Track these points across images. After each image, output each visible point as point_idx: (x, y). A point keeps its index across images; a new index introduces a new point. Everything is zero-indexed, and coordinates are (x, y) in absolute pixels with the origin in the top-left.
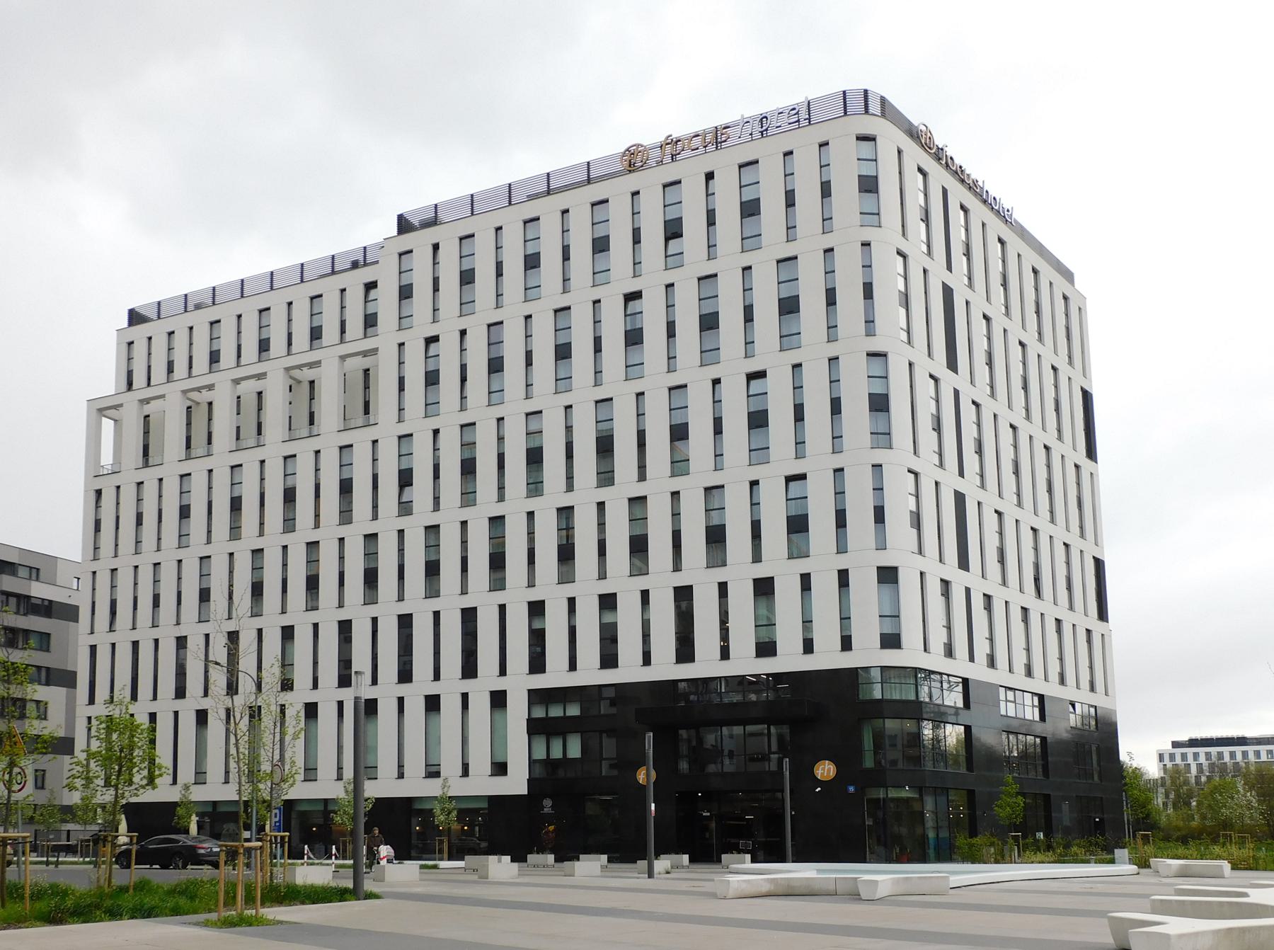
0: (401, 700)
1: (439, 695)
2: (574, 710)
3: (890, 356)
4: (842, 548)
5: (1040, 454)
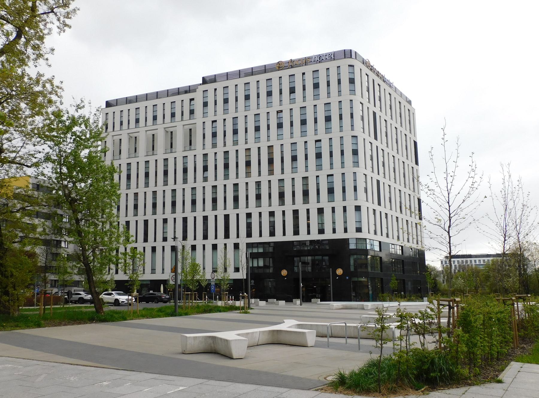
0: (204, 246)
1: (217, 244)
2: (261, 250)
3: (358, 137)
4: (344, 199)
5: (401, 164)
